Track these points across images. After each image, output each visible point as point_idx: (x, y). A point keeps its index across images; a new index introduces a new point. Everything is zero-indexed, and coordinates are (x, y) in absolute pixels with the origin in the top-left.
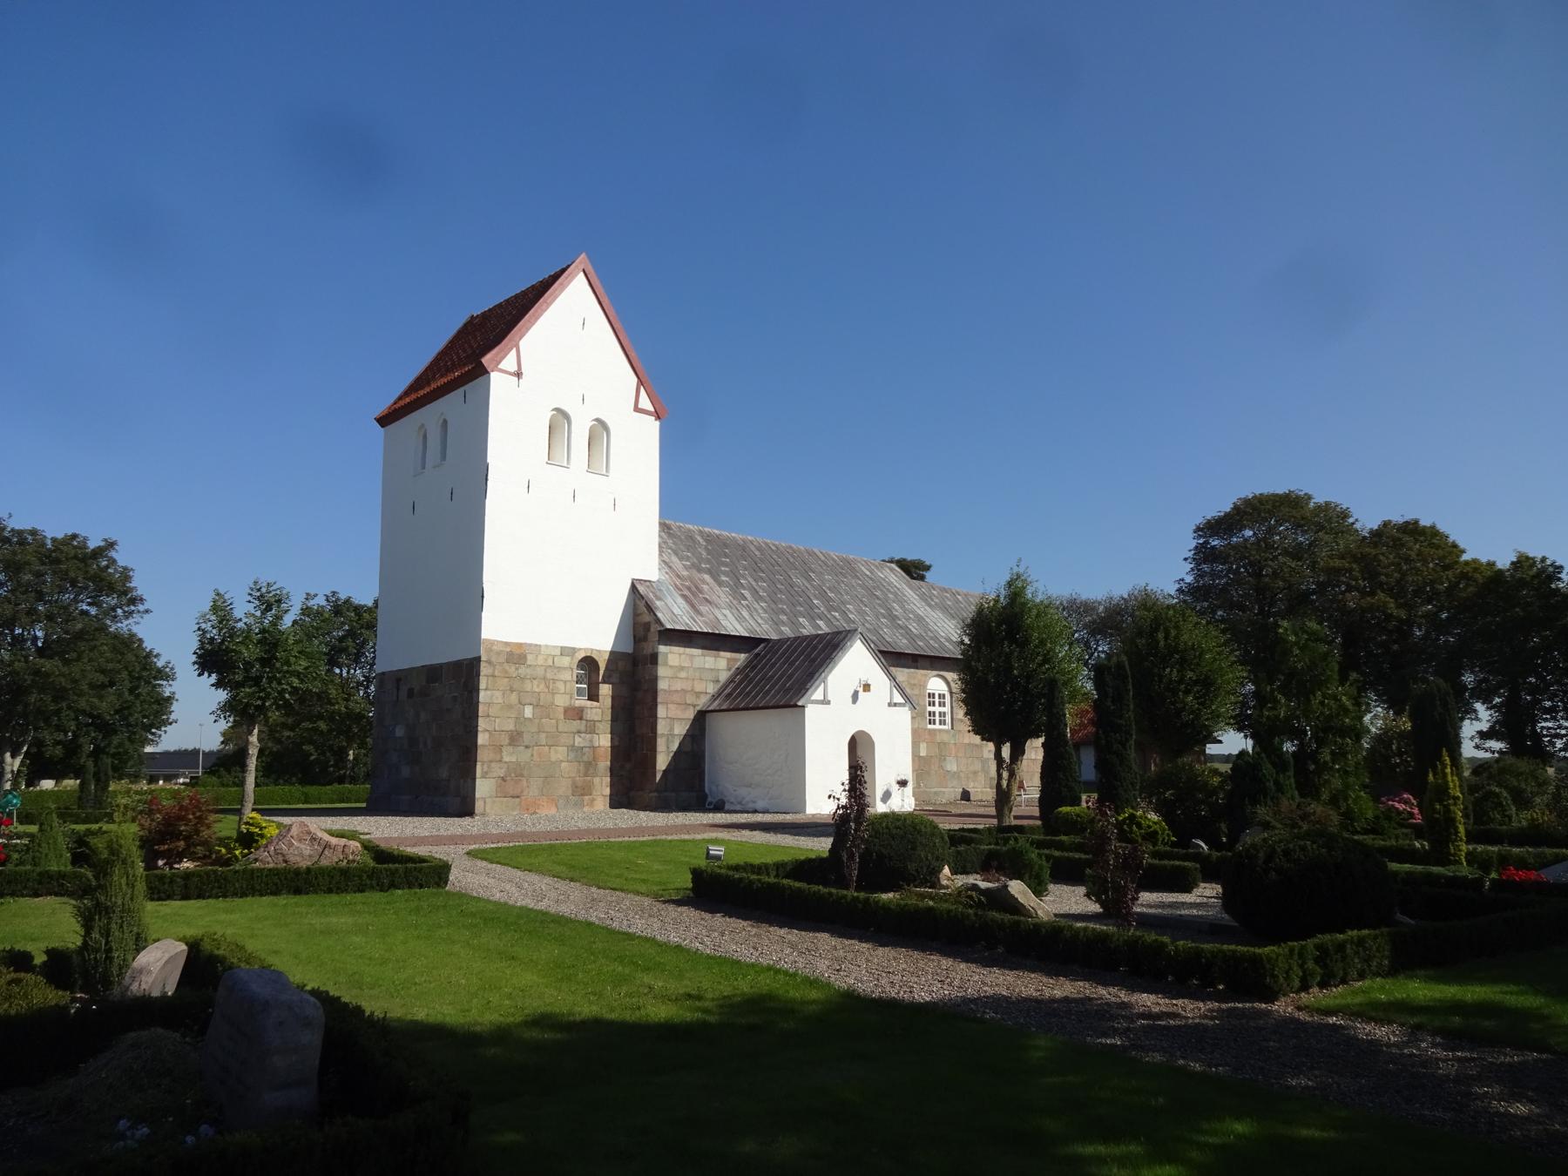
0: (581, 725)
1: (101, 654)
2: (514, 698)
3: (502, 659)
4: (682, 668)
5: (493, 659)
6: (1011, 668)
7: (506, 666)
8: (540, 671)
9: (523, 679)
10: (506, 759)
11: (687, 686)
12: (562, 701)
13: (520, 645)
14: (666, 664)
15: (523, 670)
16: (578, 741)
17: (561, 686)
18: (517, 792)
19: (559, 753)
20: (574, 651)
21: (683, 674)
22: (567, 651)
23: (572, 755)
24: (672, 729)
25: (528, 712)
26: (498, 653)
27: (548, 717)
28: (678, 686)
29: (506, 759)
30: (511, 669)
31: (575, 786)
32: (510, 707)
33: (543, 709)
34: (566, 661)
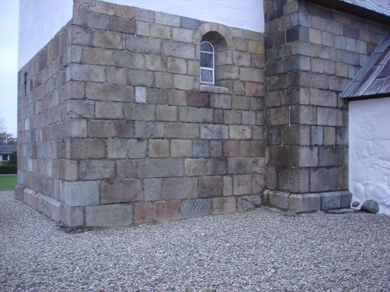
0: (208, 114)
1: (195, 214)
2: (120, 76)
3: (103, 24)
4: (324, 48)
5: (90, 24)
6: (328, 289)
7: (109, 35)
8: (155, 45)
9: (132, 52)
10: (112, 154)
11: (329, 68)
12: (183, 83)
13: (127, 9)
14: (307, 41)
15: (132, 43)
16: (205, 132)
17: (182, 66)
18: (128, 197)
19: (181, 147)
20: (200, 23)
21: (325, 55)
22: (185, 23)
23: (197, 150)
24: (315, 118)
25: (141, 95)
26: (98, 16)
27: (166, 102)
28: (320, 67)
29: (112, 154)
30: (117, 40)
31: (202, 185)
32: (115, 87)
33: (161, 94)
34: (187, 35)
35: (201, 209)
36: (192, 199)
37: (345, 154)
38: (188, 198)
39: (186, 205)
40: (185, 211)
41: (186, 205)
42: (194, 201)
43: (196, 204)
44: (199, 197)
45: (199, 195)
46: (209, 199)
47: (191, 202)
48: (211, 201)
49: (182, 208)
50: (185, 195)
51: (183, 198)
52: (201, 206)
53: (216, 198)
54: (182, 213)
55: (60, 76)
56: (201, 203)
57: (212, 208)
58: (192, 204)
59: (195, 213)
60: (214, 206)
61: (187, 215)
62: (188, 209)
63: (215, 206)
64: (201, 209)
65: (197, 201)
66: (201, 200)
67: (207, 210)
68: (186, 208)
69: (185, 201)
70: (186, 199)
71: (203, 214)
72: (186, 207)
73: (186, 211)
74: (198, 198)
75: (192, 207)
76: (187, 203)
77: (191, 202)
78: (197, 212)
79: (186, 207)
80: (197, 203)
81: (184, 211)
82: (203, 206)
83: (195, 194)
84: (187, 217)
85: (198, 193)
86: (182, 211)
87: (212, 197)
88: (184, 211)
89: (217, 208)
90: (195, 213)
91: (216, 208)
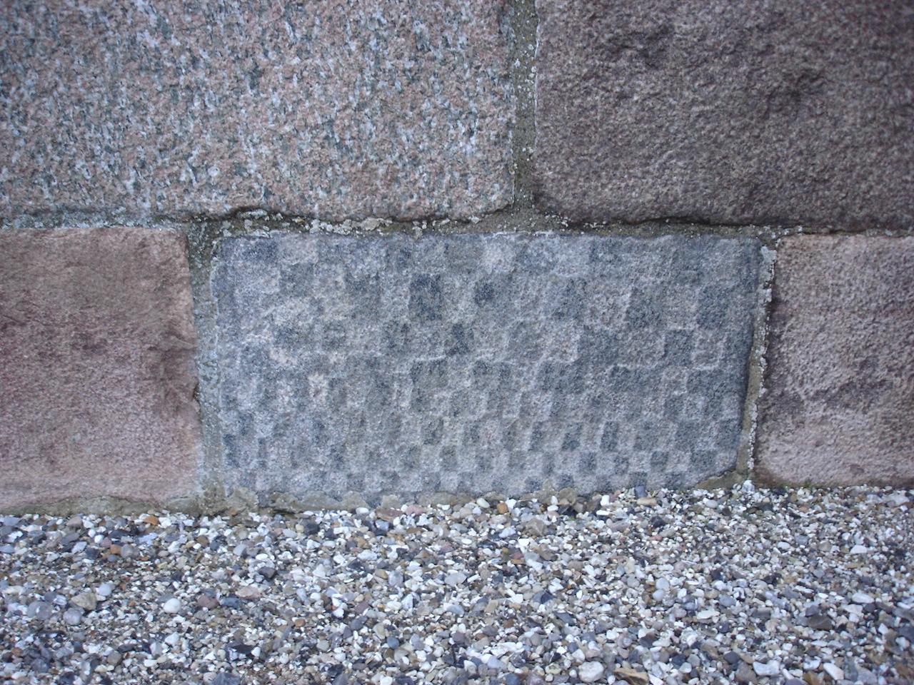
35: (559, 382)
36: (401, 222)
37: (771, 478)
38: (319, 199)
39: (289, 311)
40: (266, 400)
41: (289, 311)
42: (431, 253)
43: (461, 309)
44: (532, 204)
45: (522, 172)
46: (722, 254)
47: (371, 262)
48: (751, 284)
49: (216, 351)
50: (254, 156)
51: (217, 203)
52: (562, 343)
53: (855, 245)
54: (228, 421)
55: (67, 481)
56: (572, 304)
57: (757, 380)
58: (397, 300)
59: (454, 435)
60: (795, 356)
61: (300, 455)
62: (320, 366)
63: (814, 356)
64: (559, 382)
65: (495, 255)
66: (570, 256)
67: (672, 408)
68: (281, 358)
69: (268, 252)
70: (296, 220)
71: (589, 464)
72: (287, 337)
73: (285, 396)
74: (504, 211)
75: (398, 338)
76: (296, 282)
77: (371, 262)
78: (493, 430)
79: (287, 337)
80: (485, 294)
81: (247, 402)
82: (601, 352)
83: (461, 151)
84: (302, 477)
85: (521, 128)
86: (212, 393)
87: (780, 221)
88: (247, 402)
89: (859, 390)
90: (454, 435)
91: (830, 398)
